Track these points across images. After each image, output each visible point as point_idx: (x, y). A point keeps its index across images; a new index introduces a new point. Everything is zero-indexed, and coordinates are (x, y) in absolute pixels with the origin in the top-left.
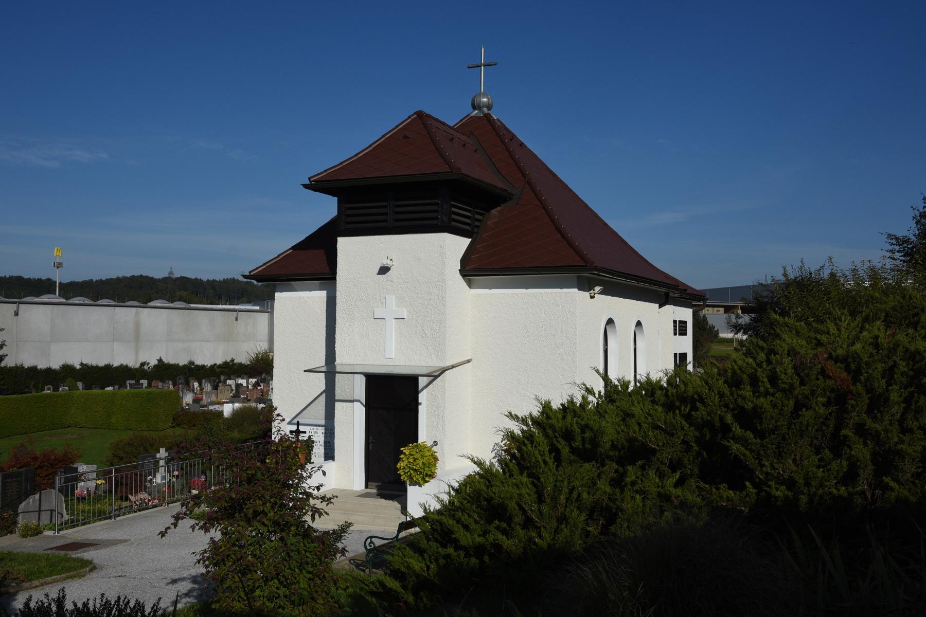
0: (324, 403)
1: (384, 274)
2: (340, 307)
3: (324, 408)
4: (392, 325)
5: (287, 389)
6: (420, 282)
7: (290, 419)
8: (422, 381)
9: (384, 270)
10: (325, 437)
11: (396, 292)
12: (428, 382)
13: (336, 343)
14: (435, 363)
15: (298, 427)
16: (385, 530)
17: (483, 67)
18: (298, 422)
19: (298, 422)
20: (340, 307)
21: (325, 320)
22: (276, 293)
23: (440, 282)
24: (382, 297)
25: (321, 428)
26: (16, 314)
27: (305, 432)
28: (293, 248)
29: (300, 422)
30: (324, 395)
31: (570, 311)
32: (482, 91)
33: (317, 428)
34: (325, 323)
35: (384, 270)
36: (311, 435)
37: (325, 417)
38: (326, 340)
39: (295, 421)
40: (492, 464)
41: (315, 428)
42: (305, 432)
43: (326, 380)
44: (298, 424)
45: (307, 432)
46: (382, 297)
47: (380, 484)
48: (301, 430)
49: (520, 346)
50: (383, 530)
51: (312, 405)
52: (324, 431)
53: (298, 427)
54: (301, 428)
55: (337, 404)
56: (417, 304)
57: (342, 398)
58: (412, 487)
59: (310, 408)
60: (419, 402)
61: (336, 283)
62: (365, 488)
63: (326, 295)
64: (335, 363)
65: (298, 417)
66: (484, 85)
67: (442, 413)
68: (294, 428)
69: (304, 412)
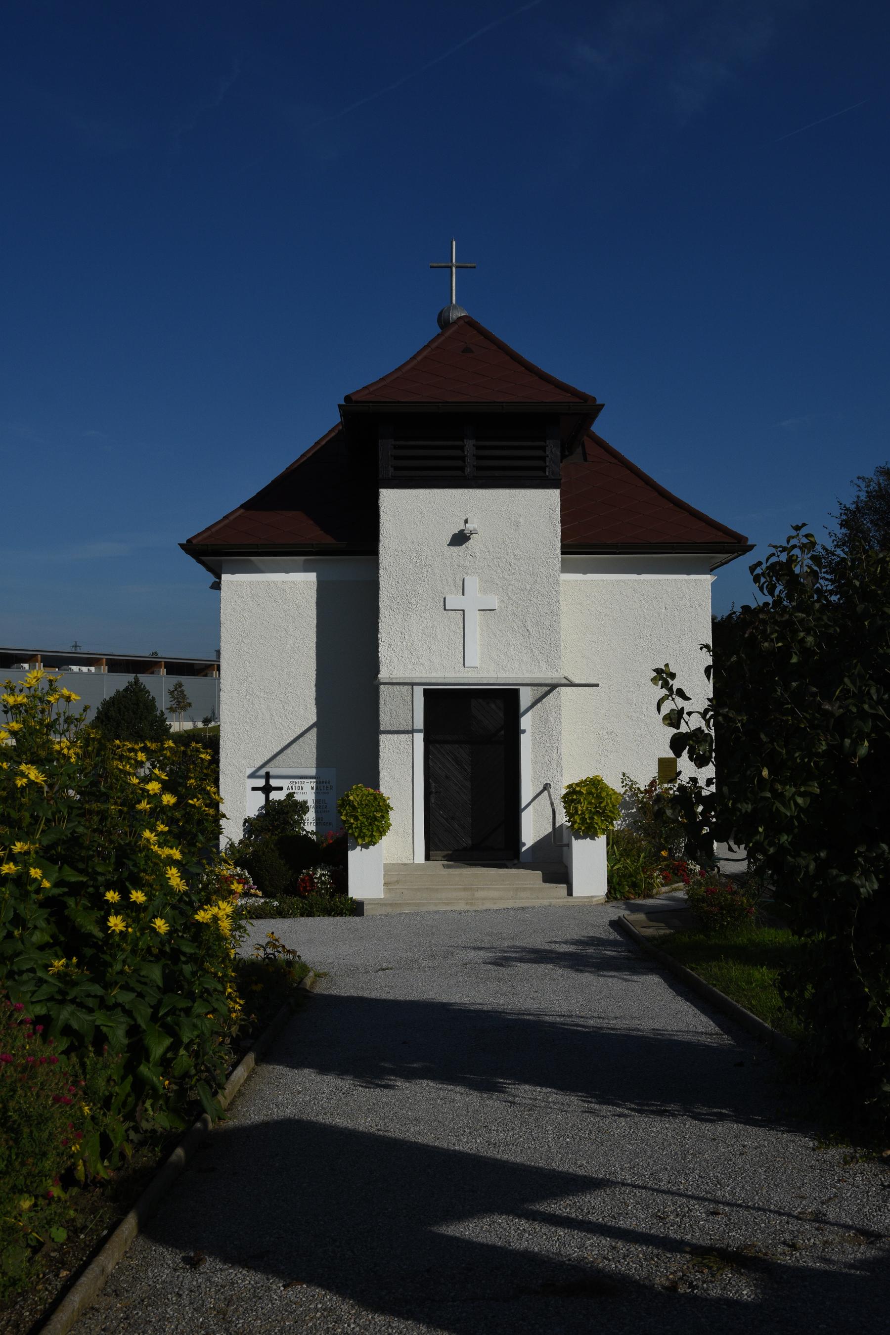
0: (315, 742)
1: (461, 545)
2: (386, 593)
3: (315, 750)
4: (474, 620)
5: (247, 723)
6: (518, 557)
7: (253, 770)
8: (526, 697)
9: (460, 539)
10: (317, 794)
11: (480, 571)
12: (534, 700)
13: (380, 647)
14: (546, 674)
15: (267, 782)
16: (551, 904)
17: (454, 269)
18: (268, 774)
19: (268, 774)
20: (386, 593)
21: (315, 617)
22: (222, 575)
23: (550, 558)
24: (458, 579)
25: (309, 781)
26: (466, 521)
27: (281, 789)
28: (243, 506)
29: (271, 774)
30: (315, 730)
31: (700, 605)
32: (454, 302)
33: (302, 780)
34: (315, 622)
35: (460, 539)
36: (291, 791)
37: (317, 764)
38: (316, 647)
39: (262, 772)
40: (106, 897)
41: (297, 780)
42: (281, 789)
43: (317, 708)
44: (268, 776)
45: (285, 788)
46: (458, 579)
47: (450, 852)
48: (273, 786)
49: (631, 653)
50: (547, 904)
51: (292, 746)
52: (314, 785)
53: (267, 782)
54: (274, 783)
55: (382, 737)
56: (514, 589)
57: (392, 729)
58: (581, 842)
59: (289, 751)
60: (522, 728)
61: (378, 560)
62: (425, 860)
63: (315, 579)
64: (379, 676)
65: (267, 766)
66: (456, 295)
67: (557, 743)
68: (261, 783)
69: (278, 758)
